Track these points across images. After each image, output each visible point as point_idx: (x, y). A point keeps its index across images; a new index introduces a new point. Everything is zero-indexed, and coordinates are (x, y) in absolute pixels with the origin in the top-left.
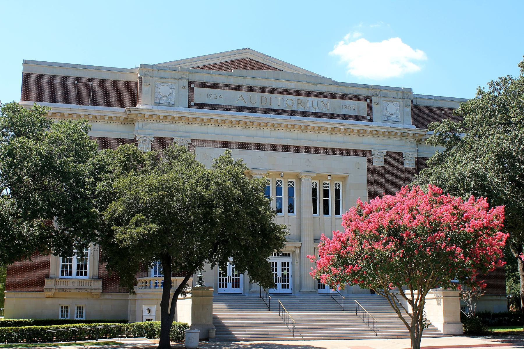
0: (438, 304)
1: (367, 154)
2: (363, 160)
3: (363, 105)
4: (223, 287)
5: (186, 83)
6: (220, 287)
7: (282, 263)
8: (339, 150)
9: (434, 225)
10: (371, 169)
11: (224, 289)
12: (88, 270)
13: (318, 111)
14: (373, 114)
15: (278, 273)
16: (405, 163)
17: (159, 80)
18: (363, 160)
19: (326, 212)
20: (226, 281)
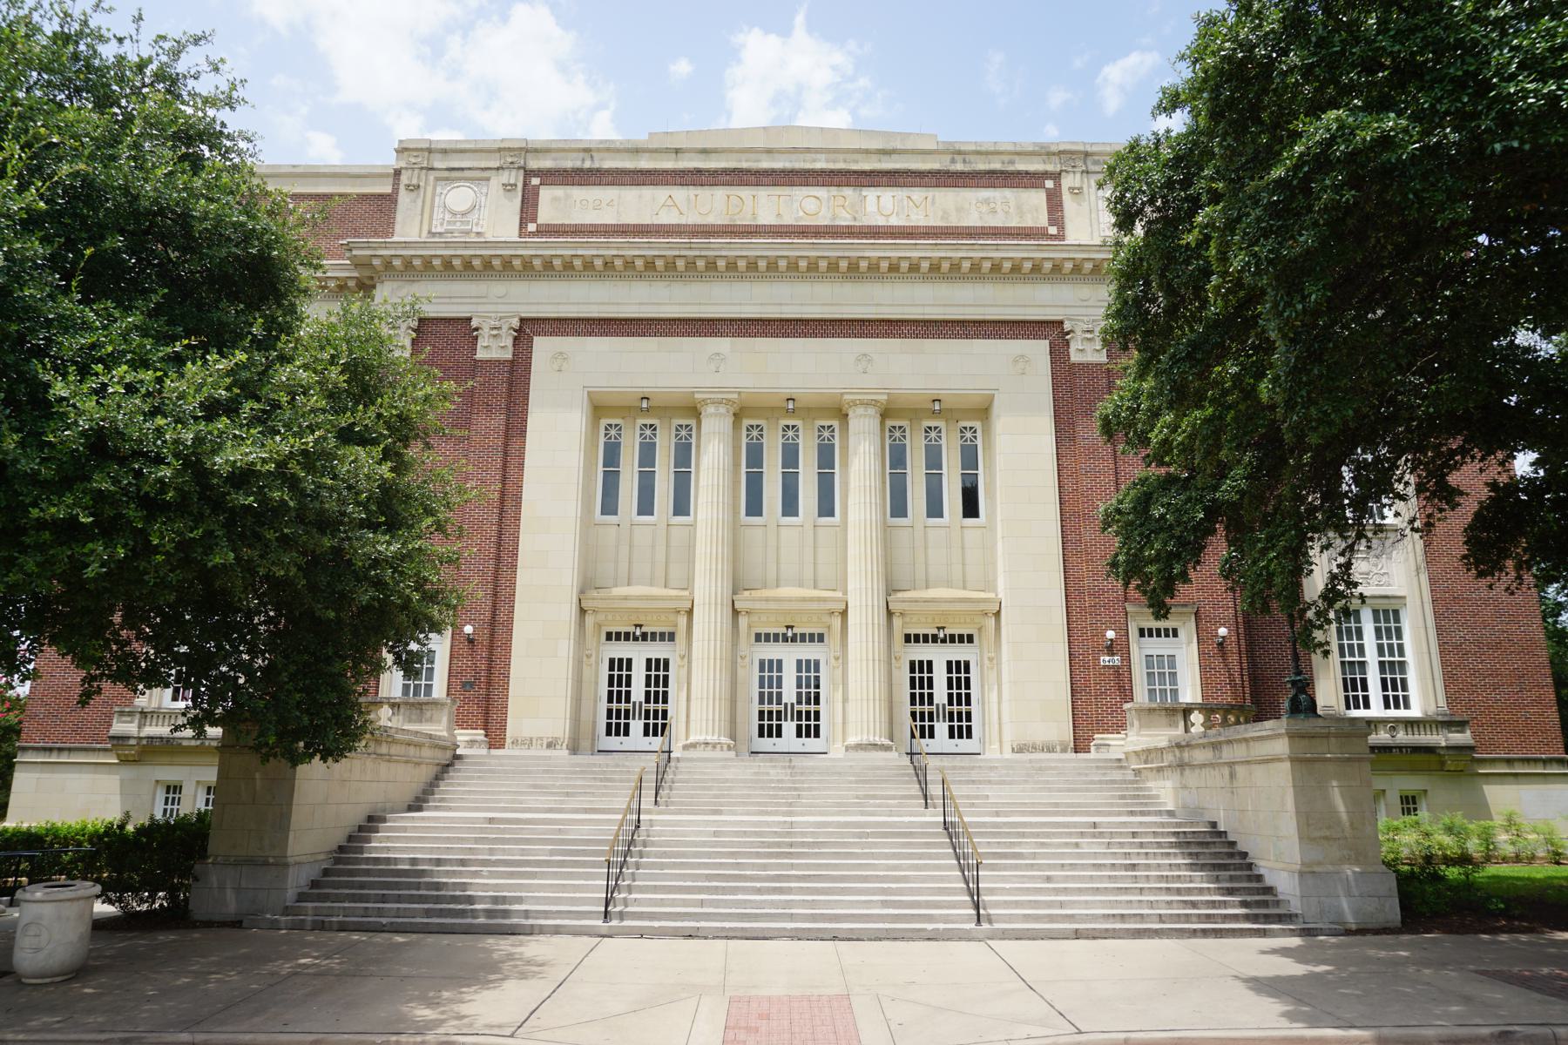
0: (1216, 832)
1: (1053, 331)
2: (1038, 350)
3: (1035, 200)
4: (770, 735)
5: (517, 178)
6: (609, 733)
7: (949, 663)
8: (805, 322)
9: (270, 535)
10: (1065, 376)
11: (775, 739)
12: (757, 674)
13: (894, 221)
14: (1067, 220)
15: (785, 690)
16: (1072, 350)
17: (446, 174)
18: (1038, 350)
19: (790, 507)
20: (931, 719)
